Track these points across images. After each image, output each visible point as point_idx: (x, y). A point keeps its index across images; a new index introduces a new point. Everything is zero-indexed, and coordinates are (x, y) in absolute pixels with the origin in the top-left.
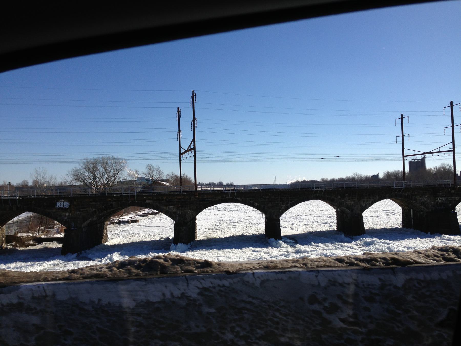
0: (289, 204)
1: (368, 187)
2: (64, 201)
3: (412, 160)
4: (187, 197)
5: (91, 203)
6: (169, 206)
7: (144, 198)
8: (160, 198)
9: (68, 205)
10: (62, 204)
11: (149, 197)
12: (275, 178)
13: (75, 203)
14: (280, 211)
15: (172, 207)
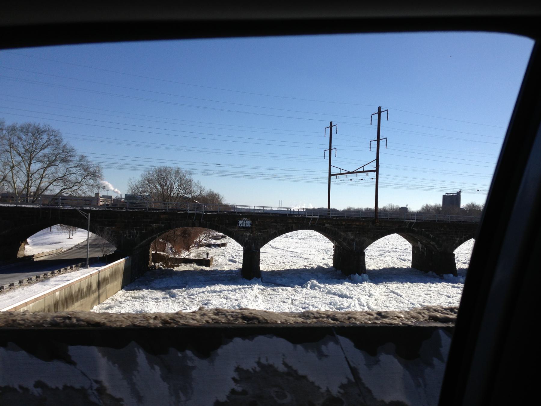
0: (463, 238)
1: (236, 213)
2: (246, 220)
3: (447, 193)
4: (365, 224)
5: (272, 224)
6: (348, 232)
7: (324, 221)
8: (339, 222)
9: (249, 224)
10: (244, 223)
11: (329, 221)
12: (280, 203)
13: (257, 223)
14: (454, 245)
15: (350, 233)
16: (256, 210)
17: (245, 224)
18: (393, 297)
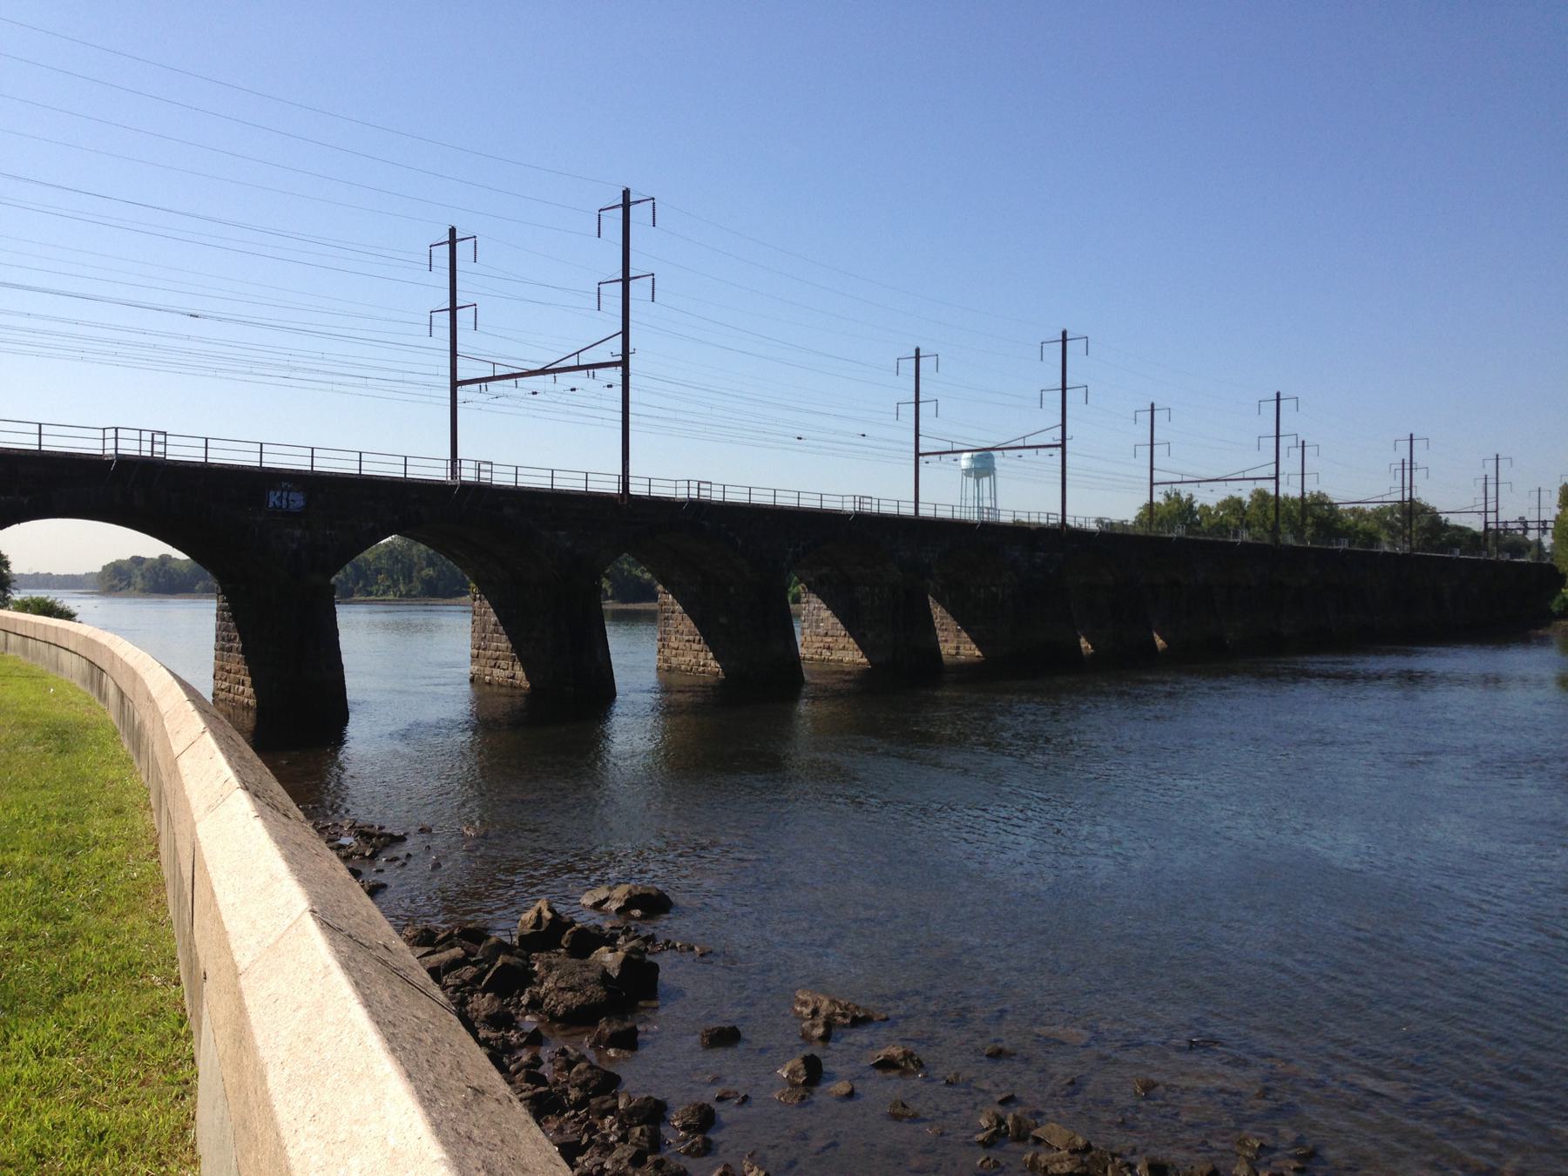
16: (107, 456)
17: (287, 499)
18: (1050, 971)
